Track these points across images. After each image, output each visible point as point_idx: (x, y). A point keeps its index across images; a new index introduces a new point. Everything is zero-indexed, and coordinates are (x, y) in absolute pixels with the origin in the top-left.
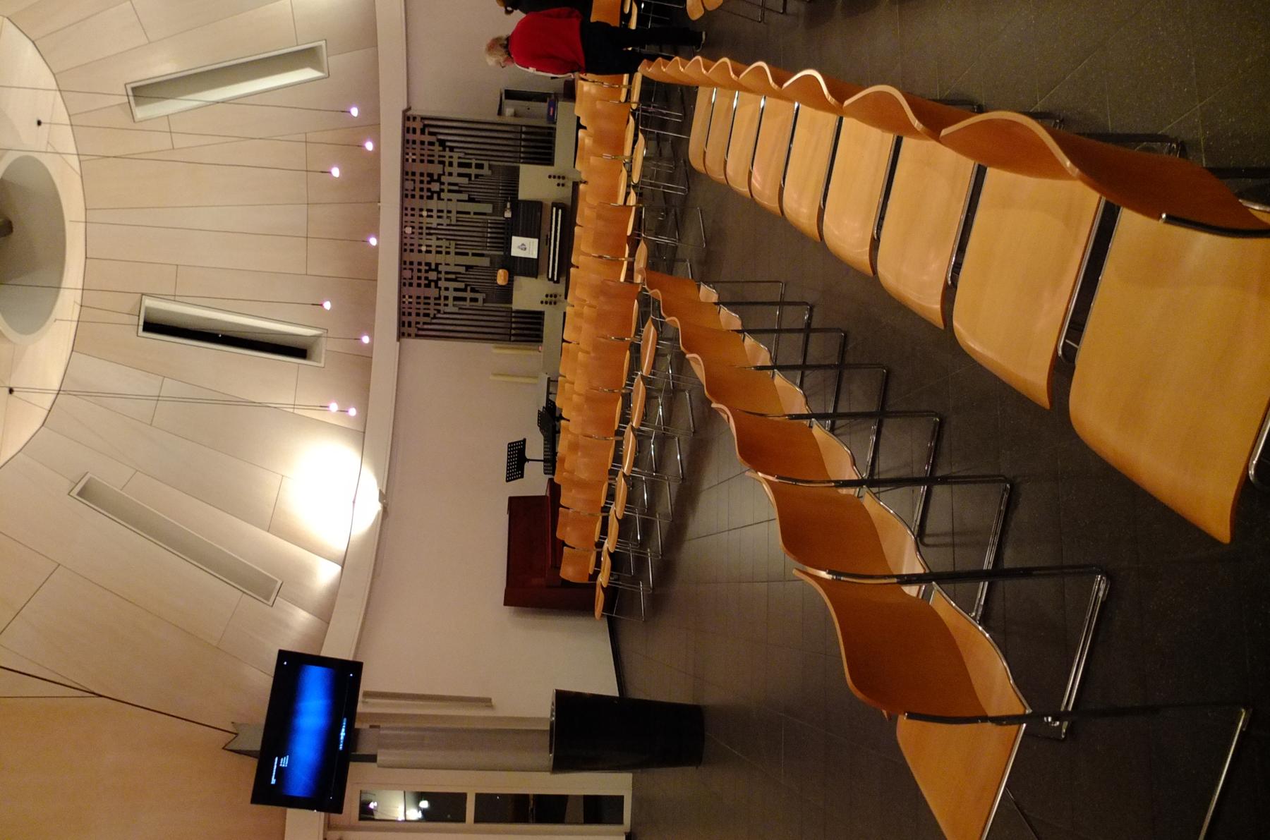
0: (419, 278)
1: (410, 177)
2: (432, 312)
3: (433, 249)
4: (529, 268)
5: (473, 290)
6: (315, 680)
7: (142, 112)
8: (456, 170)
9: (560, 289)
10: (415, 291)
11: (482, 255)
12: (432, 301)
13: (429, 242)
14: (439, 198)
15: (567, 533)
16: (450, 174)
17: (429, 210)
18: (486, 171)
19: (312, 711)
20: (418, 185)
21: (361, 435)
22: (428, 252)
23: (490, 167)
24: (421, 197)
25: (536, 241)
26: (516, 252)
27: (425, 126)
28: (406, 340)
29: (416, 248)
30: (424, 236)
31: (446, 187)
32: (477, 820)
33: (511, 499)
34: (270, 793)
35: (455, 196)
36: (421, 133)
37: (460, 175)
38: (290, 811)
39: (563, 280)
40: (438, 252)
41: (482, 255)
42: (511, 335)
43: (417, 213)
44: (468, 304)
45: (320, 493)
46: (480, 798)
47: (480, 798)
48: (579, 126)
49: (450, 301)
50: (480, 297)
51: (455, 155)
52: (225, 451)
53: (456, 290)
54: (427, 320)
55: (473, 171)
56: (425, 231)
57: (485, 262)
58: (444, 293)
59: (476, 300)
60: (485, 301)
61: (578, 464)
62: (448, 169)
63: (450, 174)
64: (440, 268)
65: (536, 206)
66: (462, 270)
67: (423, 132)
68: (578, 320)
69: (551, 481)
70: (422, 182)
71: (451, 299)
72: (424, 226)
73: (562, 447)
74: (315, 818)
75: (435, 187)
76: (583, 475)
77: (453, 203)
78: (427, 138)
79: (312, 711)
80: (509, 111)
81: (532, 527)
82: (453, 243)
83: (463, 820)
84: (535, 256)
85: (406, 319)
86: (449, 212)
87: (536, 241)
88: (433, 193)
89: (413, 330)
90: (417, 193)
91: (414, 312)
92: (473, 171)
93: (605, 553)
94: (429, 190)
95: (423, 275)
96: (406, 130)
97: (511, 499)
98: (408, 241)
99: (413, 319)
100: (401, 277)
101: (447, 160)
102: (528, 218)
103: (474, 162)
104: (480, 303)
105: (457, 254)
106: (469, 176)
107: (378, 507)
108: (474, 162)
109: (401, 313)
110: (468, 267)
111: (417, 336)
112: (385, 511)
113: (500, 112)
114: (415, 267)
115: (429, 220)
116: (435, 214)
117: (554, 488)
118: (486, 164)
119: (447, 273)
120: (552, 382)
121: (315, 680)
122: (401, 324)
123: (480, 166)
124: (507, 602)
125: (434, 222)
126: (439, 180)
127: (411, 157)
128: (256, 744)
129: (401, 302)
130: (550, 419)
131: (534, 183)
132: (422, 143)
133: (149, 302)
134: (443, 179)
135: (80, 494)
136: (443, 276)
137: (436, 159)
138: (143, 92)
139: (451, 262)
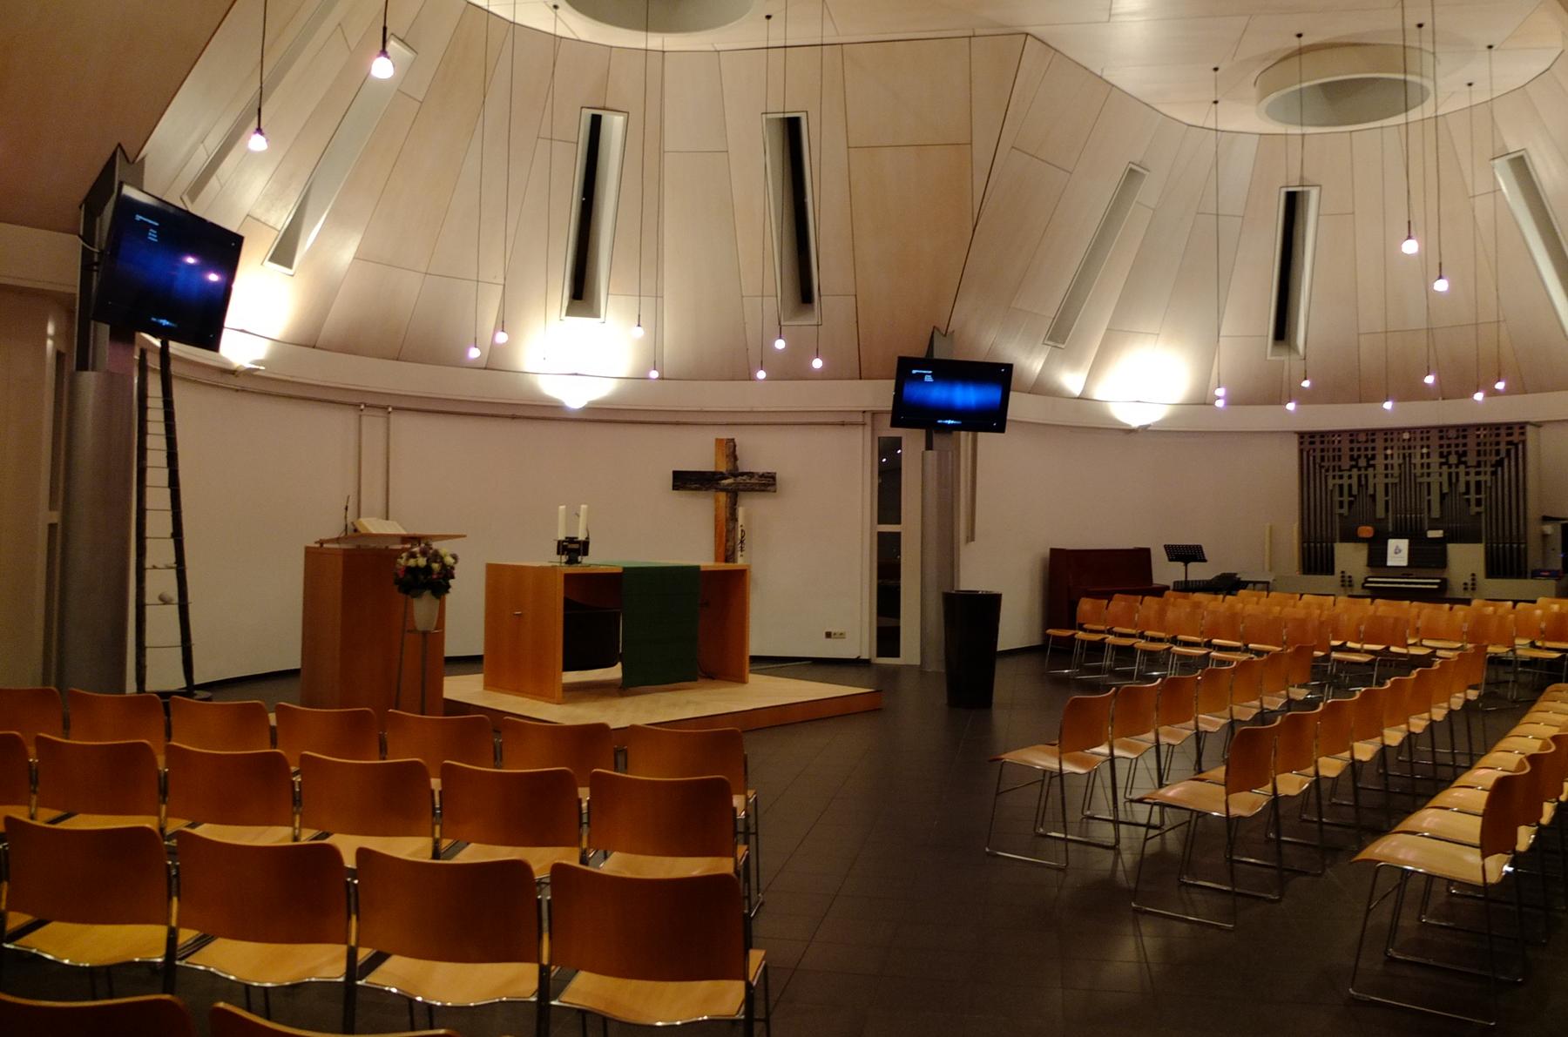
2: (1325, 464)
3: (1389, 461)
5: (1351, 503)
6: (991, 394)
7: (1501, 165)
8: (1473, 478)
9: (1358, 590)
10: (1346, 446)
12: (1337, 463)
15: (1119, 603)
16: (1467, 474)
18: (1474, 509)
19: (966, 396)
20: (1453, 442)
21: (1202, 401)
22: (1386, 457)
23: (1479, 514)
24: (1441, 446)
25: (1404, 563)
26: (1393, 544)
27: (1516, 445)
28: (1295, 439)
29: (1389, 444)
32: (880, 534)
33: (1147, 551)
34: (905, 370)
36: (1505, 442)
37: (1468, 483)
38: (892, 383)
39: (1367, 592)
40: (1386, 467)
44: (1337, 498)
45: (1144, 376)
46: (898, 535)
47: (898, 535)
48: (1516, 602)
49: (1338, 481)
50: (1345, 511)
51: (1488, 477)
52: (1179, 282)
53: (1350, 486)
55: (1473, 496)
57: (1380, 513)
58: (1346, 474)
59: (1341, 506)
60: (1341, 515)
61: (1179, 608)
62: (1472, 471)
65: (1441, 562)
66: (1371, 491)
67: (1509, 443)
68: (1341, 614)
69: (1167, 588)
73: (1198, 596)
74: (887, 404)
75: (1453, 459)
76: (1171, 614)
77: (1437, 478)
78: (1503, 447)
79: (966, 396)
80: (1548, 529)
81: (1123, 571)
83: (880, 522)
84: (1390, 563)
85: (1317, 439)
87: (1404, 563)
89: (1306, 446)
90: (1445, 442)
91: (1325, 446)
92: (1473, 496)
93: (1101, 636)
94: (1449, 453)
95: (1363, 453)
96: (1509, 426)
97: (1147, 551)
98: (1395, 435)
99: (1318, 446)
100: (1359, 431)
102: (1427, 556)
103: (1482, 496)
104: (1338, 511)
106: (1467, 492)
107: (1135, 424)
108: (1482, 496)
109: (1323, 434)
110: (1373, 497)
111: (1301, 451)
112: (1131, 431)
113: (1546, 519)
114: (1370, 445)
116: (1425, 460)
117: (1160, 591)
118: (1482, 509)
120: (1267, 587)
121: (991, 394)
122: (1312, 434)
123: (1478, 502)
124: (1053, 551)
125: (1417, 460)
126: (1460, 462)
127: (1482, 432)
128: (938, 354)
130: (1228, 584)
131: (1466, 559)
132: (1498, 443)
133: (1314, 193)
134: (1462, 467)
135: (1131, 170)
136: (1453, 470)
137: (1482, 458)
138: (1520, 165)
139: (1377, 480)
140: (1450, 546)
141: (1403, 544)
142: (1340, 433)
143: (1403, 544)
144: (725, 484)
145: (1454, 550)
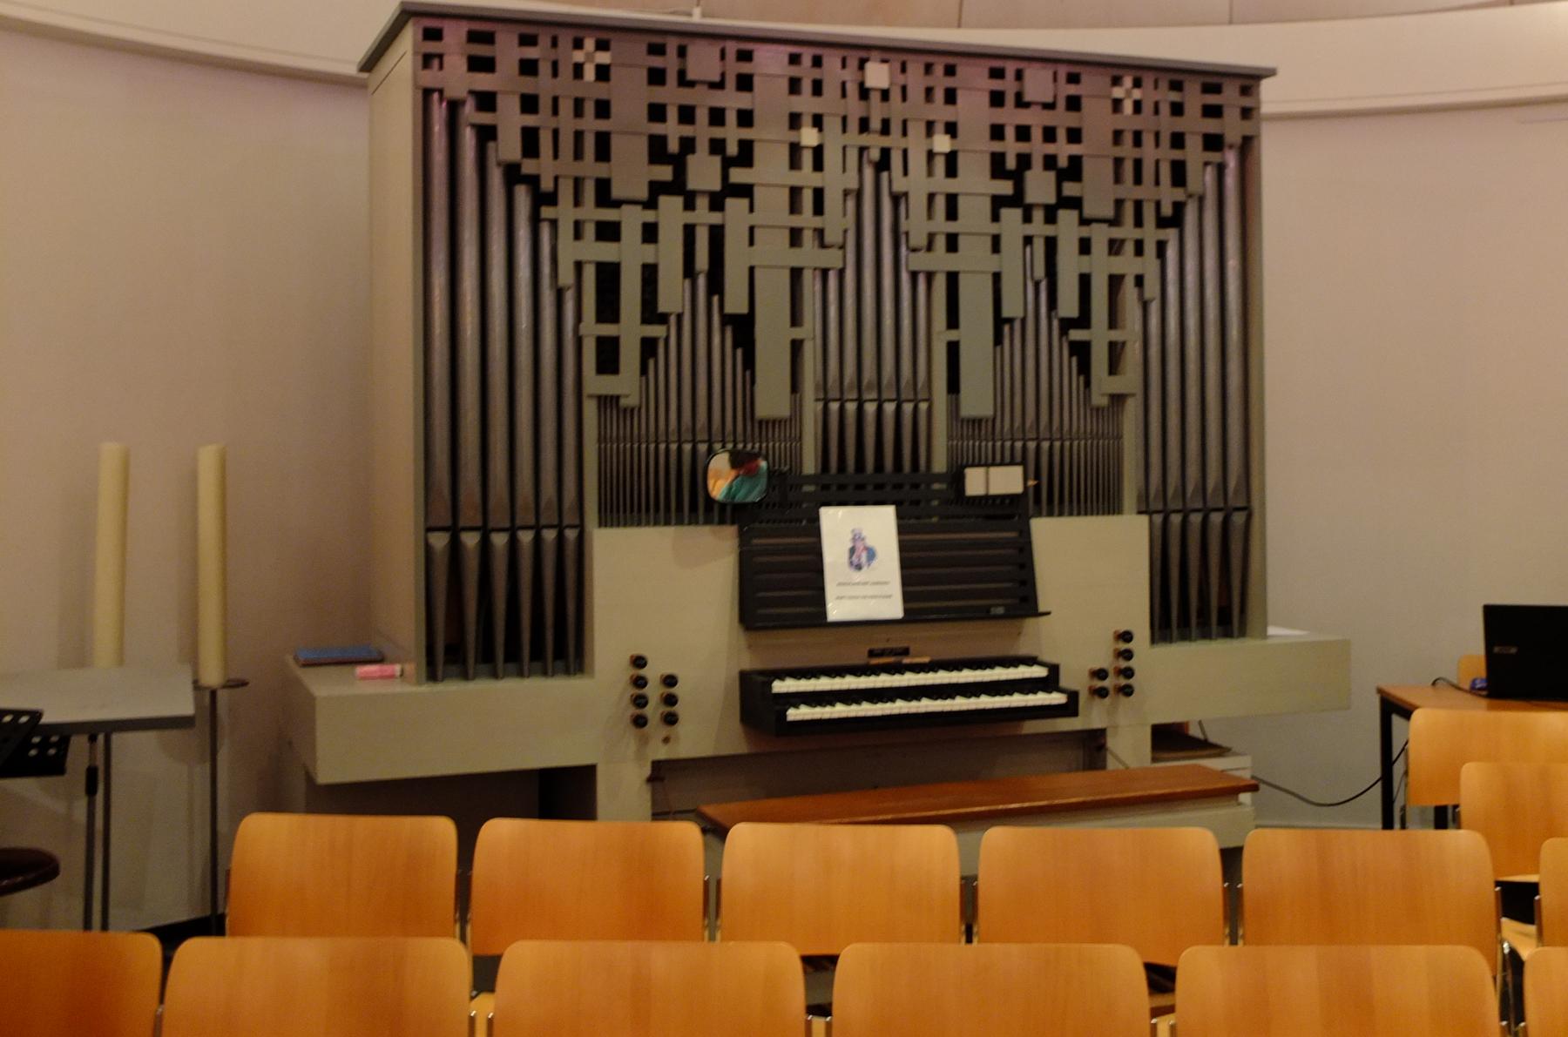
0: (687, 115)
1: (806, 72)
4: (779, 588)
5: (649, 347)
10: (630, 96)
11: (795, 386)
13: (831, 158)
14: (998, 203)
16: (1085, 247)
17: (951, 159)
23: (1118, 400)
24: (657, 113)
25: (892, 607)
26: (839, 525)
30: (855, 138)
31: (703, 216)
33: (1153, 641)
35: (1011, 262)
37: (1085, 281)
41: (795, 386)
42: (455, 531)
43: (940, 112)
53: (650, 274)
54: (508, 147)
56: (875, 142)
57: (772, 399)
58: (631, 220)
60: (608, 402)
63: (1085, 247)
64: (735, 205)
70: (1049, 135)
71: (606, 252)
72: (894, 141)
82: (831, 259)
84: (837, 610)
86: (952, 243)
88: (1017, 177)
89: (457, 78)
94: (688, 145)
95: (1037, 148)
99: (504, 80)
101: (1127, 231)
102: (971, 571)
104: (597, 384)
105: (796, 274)
106: (1083, 321)
108: (592, 329)
110: (743, 328)
115: (917, 161)
119: (717, 234)
129: (578, 30)
136: (703, 216)
140: (1046, 532)
141: (878, 524)
142: (606, 34)
143: (878, 524)
144: (1206, 164)
145: (1055, 540)
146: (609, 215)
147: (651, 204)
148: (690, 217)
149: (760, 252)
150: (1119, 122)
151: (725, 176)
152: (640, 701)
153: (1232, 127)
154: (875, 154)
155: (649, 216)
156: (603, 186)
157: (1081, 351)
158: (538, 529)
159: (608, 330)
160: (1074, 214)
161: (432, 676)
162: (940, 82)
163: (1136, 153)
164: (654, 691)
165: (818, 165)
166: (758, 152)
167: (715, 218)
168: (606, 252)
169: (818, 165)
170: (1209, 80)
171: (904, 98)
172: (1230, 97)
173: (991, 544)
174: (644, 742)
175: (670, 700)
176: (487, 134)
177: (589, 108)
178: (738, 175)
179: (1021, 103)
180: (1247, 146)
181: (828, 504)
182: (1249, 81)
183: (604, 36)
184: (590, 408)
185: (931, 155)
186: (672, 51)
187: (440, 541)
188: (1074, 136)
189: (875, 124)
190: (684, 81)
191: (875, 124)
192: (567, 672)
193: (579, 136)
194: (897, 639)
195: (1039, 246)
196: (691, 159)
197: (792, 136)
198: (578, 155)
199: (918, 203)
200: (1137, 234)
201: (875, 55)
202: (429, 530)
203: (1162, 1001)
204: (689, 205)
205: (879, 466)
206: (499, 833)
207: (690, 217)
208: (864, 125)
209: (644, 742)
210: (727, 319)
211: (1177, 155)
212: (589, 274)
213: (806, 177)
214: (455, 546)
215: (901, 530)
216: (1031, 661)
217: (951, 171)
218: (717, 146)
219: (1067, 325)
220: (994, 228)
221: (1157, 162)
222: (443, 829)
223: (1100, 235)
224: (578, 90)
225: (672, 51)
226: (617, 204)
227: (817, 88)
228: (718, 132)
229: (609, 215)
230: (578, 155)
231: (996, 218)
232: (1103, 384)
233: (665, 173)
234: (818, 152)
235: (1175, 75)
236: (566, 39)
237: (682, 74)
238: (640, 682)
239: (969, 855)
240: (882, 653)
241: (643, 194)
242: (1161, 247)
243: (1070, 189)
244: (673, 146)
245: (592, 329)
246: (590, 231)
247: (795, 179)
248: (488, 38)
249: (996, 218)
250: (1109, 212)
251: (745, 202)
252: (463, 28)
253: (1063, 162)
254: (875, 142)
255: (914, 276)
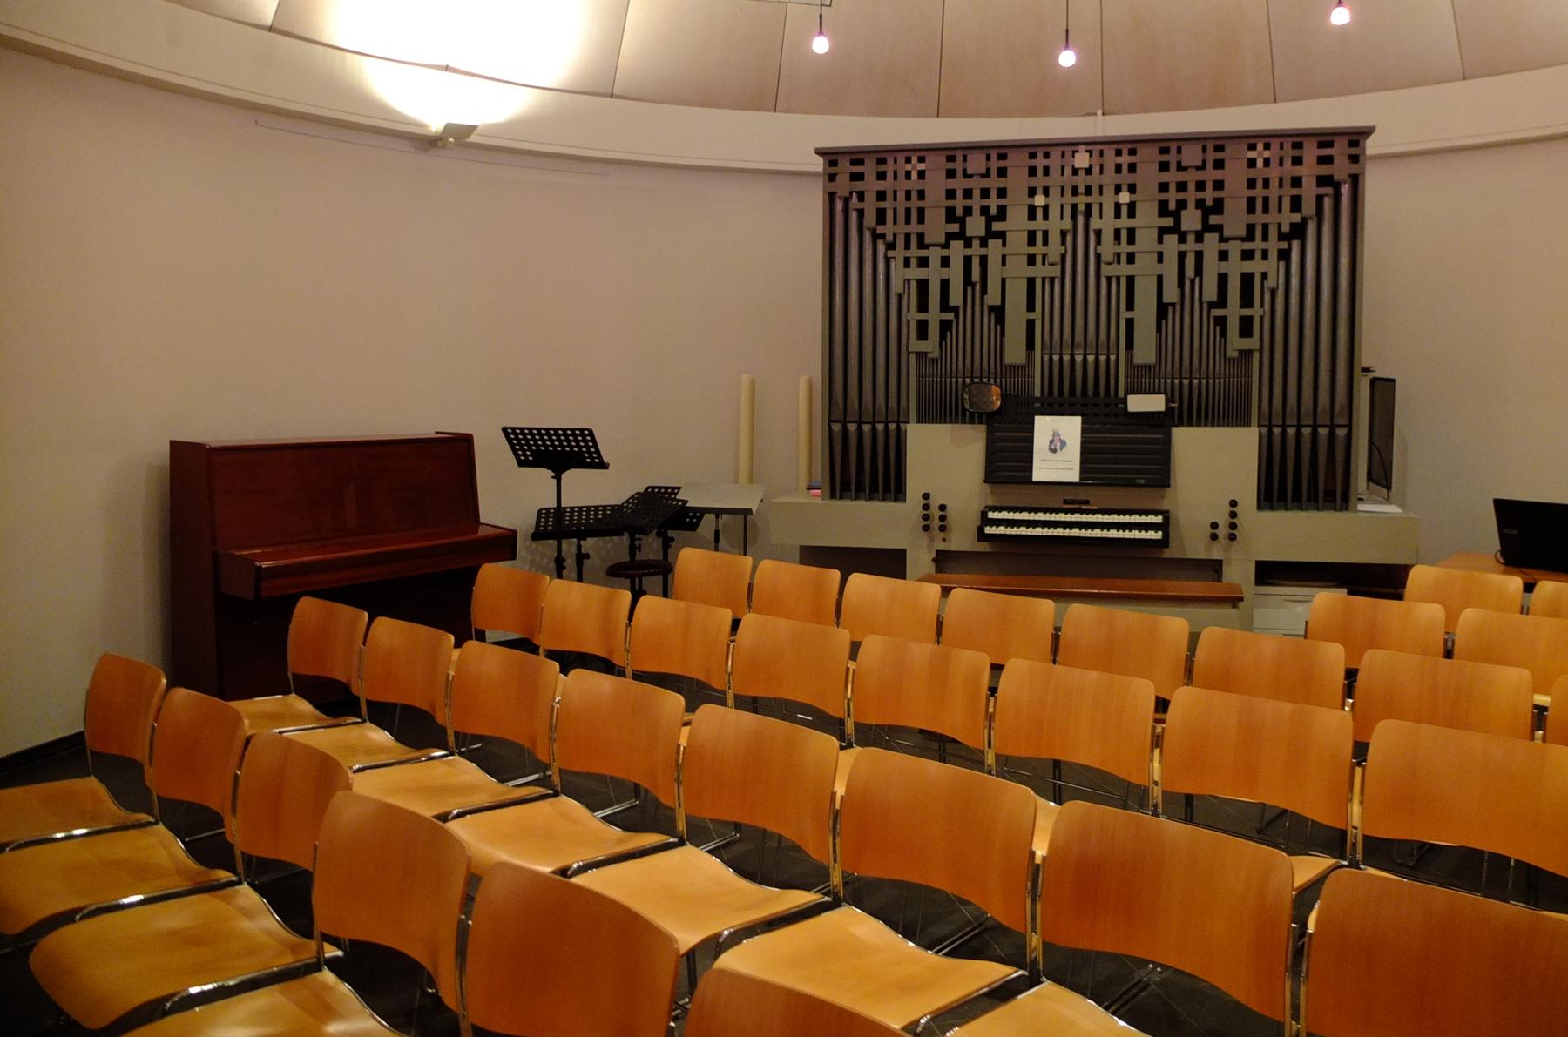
4: (1008, 463)
5: (945, 326)
11: (1030, 345)
13: (1054, 212)
14: (1163, 231)
16: (1223, 256)
17: (1132, 207)
23: (1246, 354)
24: (951, 194)
26: (1044, 426)
30: (1069, 199)
31: (1191, 246)
41: (1030, 345)
43: (1125, 178)
53: (945, 284)
54: (870, 219)
57: (1015, 352)
58: (935, 255)
60: (921, 355)
63: (1223, 256)
64: (995, 244)
71: (922, 273)
72: (1094, 198)
84: (1038, 476)
86: (1131, 258)
88: (1176, 215)
89: (843, 186)
101: (1258, 245)
102: (1129, 457)
104: (916, 345)
105: (1031, 282)
106: (1222, 302)
108: (914, 315)
110: (999, 312)
115: (1109, 210)
119: (984, 260)
136: (976, 250)
140: (1183, 437)
141: (1070, 428)
143: (1070, 428)
146: (923, 253)
147: (946, 246)
148: (968, 252)
149: (1010, 270)
150: (1252, 173)
151: (988, 226)
152: (926, 517)
153: (1340, 169)
154: (1081, 208)
155: (945, 252)
156: (921, 237)
157: (1221, 322)
158: (886, 423)
159: (922, 316)
160: (1216, 236)
161: (833, 496)
162: (1212, 156)
163: (1265, 193)
164: (937, 513)
165: (1046, 217)
166: (1227, 204)
167: (983, 251)
168: (922, 273)
169: (1046, 217)
170: (1323, 139)
171: (1101, 172)
172: (1339, 151)
173: (1144, 441)
174: (932, 539)
175: (943, 518)
176: (861, 213)
177: (914, 195)
178: (997, 226)
179: (1180, 168)
180: (1355, 180)
181: (1159, 413)
182: (1357, 137)
183: (922, 154)
184: (913, 358)
185: (1118, 206)
186: (959, 159)
187: (837, 427)
188: (1219, 185)
189: (1081, 189)
190: (966, 175)
191: (1081, 189)
192: (896, 500)
193: (908, 211)
194: (1081, 494)
195: (976, 263)
196: (1183, 213)
197: (1029, 201)
198: (908, 221)
199: (1108, 237)
200: (1264, 245)
201: (1082, 148)
202: (831, 421)
203: (1160, 716)
204: (968, 244)
205: (1096, 392)
206: (857, 579)
207: (968, 252)
208: (1075, 192)
209: (932, 539)
210: (991, 308)
211: (1295, 191)
212: (914, 285)
213: (1039, 224)
214: (845, 430)
215: (1084, 431)
216: (1156, 513)
217: (1132, 214)
218: (985, 211)
219: (1212, 305)
220: (1160, 248)
221: (1280, 198)
222: (835, 575)
223: (1235, 249)
224: (907, 185)
225: (959, 159)
226: (927, 247)
227: (1046, 171)
228: (985, 202)
229: (923, 253)
230: (908, 221)
231: (1160, 241)
232: (1235, 343)
233: (1168, 222)
234: (1046, 208)
235: (1297, 139)
236: (901, 158)
237: (1179, 163)
238: (926, 507)
239: (1059, 615)
240: (1072, 502)
241: (943, 241)
242: (1284, 255)
243: (1214, 219)
244: (1172, 206)
245: (914, 315)
246: (914, 262)
247: (1032, 225)
248: (861, 162)
249: (1160, 241)
250: (1243, 233)
251: (1000, 242)
252: (848, 157)
253: (1209, 203)
254: (1081, 201)
255: (1109, 279)
